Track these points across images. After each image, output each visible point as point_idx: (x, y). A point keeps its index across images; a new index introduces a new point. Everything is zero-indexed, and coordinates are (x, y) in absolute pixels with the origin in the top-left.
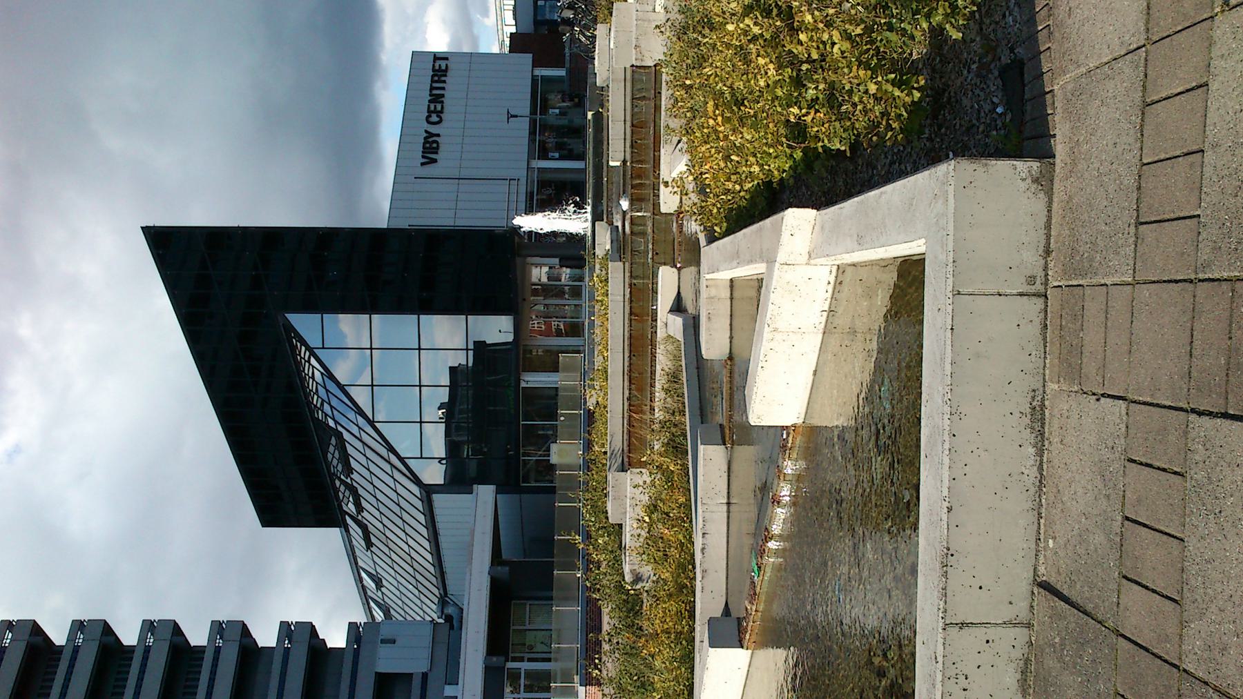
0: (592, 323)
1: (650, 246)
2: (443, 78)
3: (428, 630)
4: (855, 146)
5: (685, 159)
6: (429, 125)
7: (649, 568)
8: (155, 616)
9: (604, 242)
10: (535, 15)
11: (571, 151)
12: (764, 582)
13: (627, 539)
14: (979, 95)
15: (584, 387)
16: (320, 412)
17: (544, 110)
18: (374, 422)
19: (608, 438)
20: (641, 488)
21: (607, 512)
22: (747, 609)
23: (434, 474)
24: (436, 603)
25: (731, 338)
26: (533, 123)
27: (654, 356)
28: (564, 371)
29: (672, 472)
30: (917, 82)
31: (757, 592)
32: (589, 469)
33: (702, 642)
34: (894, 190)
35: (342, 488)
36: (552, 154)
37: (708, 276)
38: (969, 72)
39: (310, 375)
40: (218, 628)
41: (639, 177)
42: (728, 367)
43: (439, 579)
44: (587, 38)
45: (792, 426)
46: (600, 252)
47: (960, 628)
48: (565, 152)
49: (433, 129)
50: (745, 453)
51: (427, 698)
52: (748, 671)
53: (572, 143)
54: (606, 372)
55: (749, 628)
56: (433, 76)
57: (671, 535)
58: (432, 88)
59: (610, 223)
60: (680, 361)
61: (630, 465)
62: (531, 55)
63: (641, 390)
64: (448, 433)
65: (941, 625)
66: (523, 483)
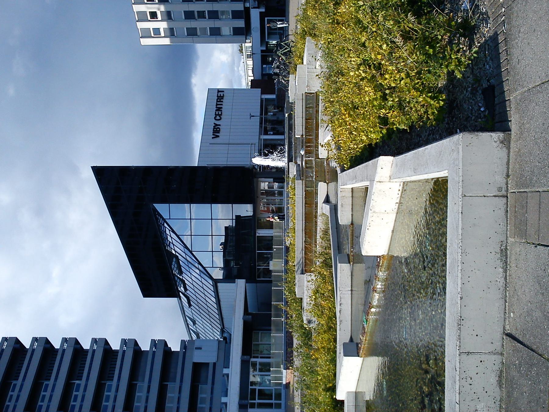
0: (288, 208)
2: (222, 100)
3: (217, 343)
4: (412, 127)
6: (216, 121)
8: (98, 336)
9: (293, 171)
11: (278, 131)
12: (369, 327)
13: (305, 305)
14: (472, 102)
16: (168, 247)
18: (192, 251)
19: (296, 259)
21: (295, 292)
22: (361, 339)
23: (218, 274)
25: (352, 215)
26: (261, 119)
27: (316, 222)
29: (325, 275)
30: (442, 97)
32: (287, 273)
33: (340, 353)
34: (432, 147)
35: (178, 281)
38: (467, 92)
39: (164, 231)
40: (124, 342)
43: (221, 321)
44: (285, 81)
46: (291, 176)
47: (468, 355)
48: (275, 132)
49: (217, 123)
52: (361, 367)
53: (279, 128)
54: (295, 229)
56: (217, 99)
58: (217, 105)
59: (296, 163)
60: (329, 225)
61: (306, 271)
62: (260, 89)
63: (310, 238)
64: (224, 256)
65: (458, 353)
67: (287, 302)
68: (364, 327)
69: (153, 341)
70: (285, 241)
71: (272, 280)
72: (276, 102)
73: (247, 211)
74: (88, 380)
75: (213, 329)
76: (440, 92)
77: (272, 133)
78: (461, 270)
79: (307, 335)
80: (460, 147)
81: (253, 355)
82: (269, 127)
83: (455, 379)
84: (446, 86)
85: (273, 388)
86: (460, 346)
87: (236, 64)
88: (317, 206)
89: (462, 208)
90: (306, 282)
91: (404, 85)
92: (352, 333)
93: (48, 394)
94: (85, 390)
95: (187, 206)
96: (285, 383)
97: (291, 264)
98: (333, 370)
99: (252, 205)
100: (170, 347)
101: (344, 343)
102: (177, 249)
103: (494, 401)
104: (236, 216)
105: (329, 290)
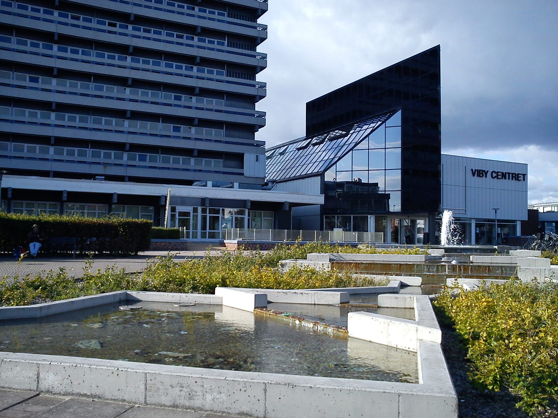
0: (396, 247)
1: (431, 274)
2: (514, 179)
3: (262, 176)
4: (469, 361)
5: (469, 289)
7: (288, 271)
8: (269, 59)
9: (435, 253)
10: (548, 222)
11: (480, 238)
12: (282, 318)
13: (300, 261)
14: (490, 414)
15: (368, 244)
16: (357, 126)
17: (499, 226)
18: (352, 150)
19: (345, 254)
20: (322, 267)
21: (312, 253)
22: (271, 310)
23: (329, 177)
24: (273, 179)
25: (387, 308)
26: (493, 221)
27: (381, 274)
28: (375, 234)
29: (329, 281)
30: (496, 388)
31: (277, 315)
32: (331, 245)
33: (257, 292)
34: (446, 373)
35: (323, 137)
36: (478, 230)
37: (415, 298)
38: (502, 411)
39: (373, 122)
40: (263, 86)
41: (464, 270)
42: (374, 306)
43: (283, 180)
44: (534, 246)
45: (348, 331)
46: (430, 251)
47: (264, 390)
48: (480, 236)
49: (489, 175)
50: (337, 313)
51: (1, 42)
52: (245, 311)
53: (485, 238)
54: (374, 253)
55: (263, 311)
56: (515, 174)
57: (301, 280)
58: (509, 174)
59: (443, 256)
60: (378, 286)
61: (332, 263)
62: (527, 220)
63: (366, 268)
64: (347, 182)
65: (266, 382)
66: (325, 216)
67: (301, 245)
68: (282, 313)
69: (264, 114)
70: (362, 244)
71: (323, 230)
72: (512, 236)
73: (394, 205)
74: (228, 53)
75: (276, 173)
76: (502, 388)
77: (478, 232)
78: (335, 389)
79: (272, 263)
80: (444, 395)
81: (251, 211)
82: (485, 229)
83: (244, 378)
84: (509, 395)
85: (220, 231)
86: (271, 384)
87: (556, 193)
88: (397, 276)
89: (388, 393)
90: (322, 262)
91: (512, 356)
92: (275, 304)
93: (216, 16)
94: (219, 50)
95: (399, 143)
96: (225, 242)
97: (340, 249)
98: (241, 285)
99: (400, 211)
100: (258, 131)
101: (267, 295)
102: (355, 135)
103: (228, 408)
104: (390, 194)
105: (314, 284)
